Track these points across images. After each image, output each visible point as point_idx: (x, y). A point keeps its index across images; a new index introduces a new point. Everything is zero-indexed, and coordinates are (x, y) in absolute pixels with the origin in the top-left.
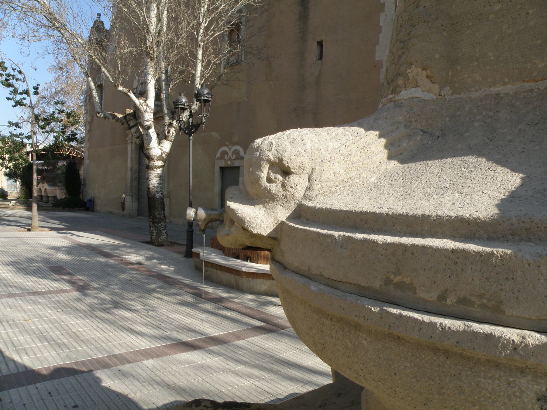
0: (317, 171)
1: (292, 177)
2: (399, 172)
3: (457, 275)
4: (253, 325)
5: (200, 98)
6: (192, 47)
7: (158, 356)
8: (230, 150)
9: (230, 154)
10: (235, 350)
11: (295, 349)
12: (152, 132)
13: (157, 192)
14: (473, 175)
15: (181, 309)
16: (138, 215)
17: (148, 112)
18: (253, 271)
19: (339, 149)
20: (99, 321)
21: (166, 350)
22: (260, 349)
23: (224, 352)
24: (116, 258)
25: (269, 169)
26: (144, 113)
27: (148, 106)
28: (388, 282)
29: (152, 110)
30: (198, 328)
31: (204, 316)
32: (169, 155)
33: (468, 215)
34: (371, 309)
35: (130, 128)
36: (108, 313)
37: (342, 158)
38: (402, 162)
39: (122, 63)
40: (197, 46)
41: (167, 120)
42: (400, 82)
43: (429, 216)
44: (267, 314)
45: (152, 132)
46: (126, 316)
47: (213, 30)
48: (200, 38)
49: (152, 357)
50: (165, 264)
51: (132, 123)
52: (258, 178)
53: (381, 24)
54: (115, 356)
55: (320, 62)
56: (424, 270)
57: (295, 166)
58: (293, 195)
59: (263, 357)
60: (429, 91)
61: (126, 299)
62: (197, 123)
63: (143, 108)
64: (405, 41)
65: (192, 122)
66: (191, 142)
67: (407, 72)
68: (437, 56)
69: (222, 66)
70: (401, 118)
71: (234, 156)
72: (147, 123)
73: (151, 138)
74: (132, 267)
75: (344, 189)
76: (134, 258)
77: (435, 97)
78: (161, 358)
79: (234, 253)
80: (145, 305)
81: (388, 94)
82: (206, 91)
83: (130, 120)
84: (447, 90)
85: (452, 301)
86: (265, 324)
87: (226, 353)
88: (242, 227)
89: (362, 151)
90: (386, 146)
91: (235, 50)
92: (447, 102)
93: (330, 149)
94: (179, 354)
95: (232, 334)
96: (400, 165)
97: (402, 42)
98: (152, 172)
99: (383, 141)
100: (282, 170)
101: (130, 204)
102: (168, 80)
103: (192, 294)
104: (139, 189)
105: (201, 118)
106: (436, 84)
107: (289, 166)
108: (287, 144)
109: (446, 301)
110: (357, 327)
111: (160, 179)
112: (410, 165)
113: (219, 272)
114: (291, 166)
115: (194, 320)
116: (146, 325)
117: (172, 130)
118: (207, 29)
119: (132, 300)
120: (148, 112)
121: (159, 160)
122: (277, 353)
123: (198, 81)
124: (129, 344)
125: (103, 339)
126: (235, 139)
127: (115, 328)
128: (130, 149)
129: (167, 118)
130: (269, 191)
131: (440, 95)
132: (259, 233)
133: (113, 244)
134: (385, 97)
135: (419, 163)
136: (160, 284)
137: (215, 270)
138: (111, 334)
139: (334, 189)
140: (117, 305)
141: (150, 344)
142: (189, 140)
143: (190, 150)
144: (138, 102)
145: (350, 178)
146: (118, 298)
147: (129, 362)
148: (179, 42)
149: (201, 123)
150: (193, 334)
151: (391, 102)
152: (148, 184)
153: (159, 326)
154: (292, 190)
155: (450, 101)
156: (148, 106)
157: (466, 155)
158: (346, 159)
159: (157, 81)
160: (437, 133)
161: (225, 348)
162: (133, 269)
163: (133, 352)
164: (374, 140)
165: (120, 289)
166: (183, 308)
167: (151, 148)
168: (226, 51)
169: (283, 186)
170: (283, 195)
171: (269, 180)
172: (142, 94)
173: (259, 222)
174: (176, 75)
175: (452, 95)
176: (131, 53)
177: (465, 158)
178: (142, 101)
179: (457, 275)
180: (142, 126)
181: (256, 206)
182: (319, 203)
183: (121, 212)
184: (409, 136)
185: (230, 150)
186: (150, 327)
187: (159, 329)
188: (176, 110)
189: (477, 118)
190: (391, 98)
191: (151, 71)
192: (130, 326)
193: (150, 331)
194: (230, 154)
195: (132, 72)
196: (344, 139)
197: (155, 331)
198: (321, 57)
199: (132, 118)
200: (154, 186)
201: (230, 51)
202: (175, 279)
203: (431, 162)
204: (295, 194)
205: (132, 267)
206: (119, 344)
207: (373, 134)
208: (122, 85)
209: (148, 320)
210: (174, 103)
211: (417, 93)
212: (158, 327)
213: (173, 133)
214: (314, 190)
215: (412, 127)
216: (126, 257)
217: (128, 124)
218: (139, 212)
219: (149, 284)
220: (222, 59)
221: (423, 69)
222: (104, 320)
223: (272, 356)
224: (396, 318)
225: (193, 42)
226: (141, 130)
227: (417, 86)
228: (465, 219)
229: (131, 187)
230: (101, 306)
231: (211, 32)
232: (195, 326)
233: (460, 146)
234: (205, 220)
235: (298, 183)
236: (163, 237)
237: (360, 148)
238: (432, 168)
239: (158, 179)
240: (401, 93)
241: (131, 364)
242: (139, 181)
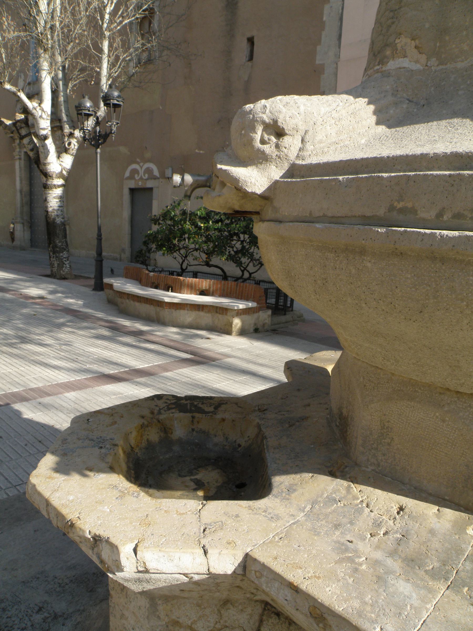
0: (310, 133)
1: (286, 138)
2: (388, 135)
3: (453, 195)
4: (180, 357)
5: (108, 102)
6: (97, 37)
7: (80, 389)
8: (141, 167)
9: (141, 172)
10: (163, 381)
11: (229, 380)
12: (49, 143)
13: (57, 216)
14: (459, 131)
15: (97, 342)
16: (32, 246)
17: (44, 119)
18: (176, 301)
19: (330, 113)
20: (7, 356)
21: (87, 383)
22: (191, 380)
23: (152, 383)
24: (13, 292)
25: (263, 130)
26: (39, 119)
27: (42, 111)
28: (392, 208)
29: (48, 116)
30: (120, 361)
31: (124, 349)
32: (70, 172)
33: (461, 151)
34: (378, 231)
35: (22, 138)
36: (15, 348)
37: (333, 121)
38: (389, 127)
39: (6, 53)
40: (102, 36)
41: (67, 129)
42: (388, 53)
43: (427, 154)
44: (194, 346)
45: (49, 143)
46: (36, 350)
47: (122, 16)
48: (105, 25)
49: (74, 390)
50: (71, 298)
51: (23, 132)
52: (251, 140)
53: (324, 19)
54: (32, 390)
55: (250, 64)
56: (425, 194)
57: (289, 128)
58: (287, 155)
59: (195, 388)
60: (417, 62)
61: (33, 334)
62: (106, 133)
63: (38, 113)
64: (396, 10)
65: (100, 132)
66: (99, 155)
67: (396, 42)
68: (427, 25)
69: (131, 64)
70: (388, 87)
71: (147, 175)
72: (43, 132)
73: (48, 151)
74: (34, 301)
75: (336, 150)
76: (34, 291)
77: (422, 68)
78: (83, 390)
79: (153, 283)
80: (57, 339)
81: (375, 66)
82: (116, 94)
83: (21, 128)
84: (433, 61)
85: (448, 217)
86: (193, 356)
87: (155, 384)
88: (235, 187)
89: (352, 116)
90: (375, 113)
91: (149, 43)
92: (432, 73)
93: (322, 113)
94: (103, 387)
95: (158, 366)
96: (388, 130)
97: (392, 11)
98: (50, 192)
99: (372, 107)
100: (275, 132)
101: (21, 233)
102: (66, 80)
103: (107, 327)
104: (31, 216)
105: (111, 126)
106: (424, 55)
107: (284, 127)
108: (281, 106)
109: (443, 218)
110: (363, 252)
111: (60, 201)
112: (398, 129)
113: (137, 304)
114: (285, 128)
115: (114, 353)
116: (61, 359)
117: (74, 141)
118: (114, 14)
119: (40, 334)
120: (44, 119)
121: (59, 177)
122: (209, 384)
123: (105, 83)
124: (46, 378)
125: (15, 373)
126: (148, 155)
127: (27, 363)
128: (19, 166)
129: (67, 126)
130: (263, 152)
131: (426, 66)
132: (253, 191)
133: (6, 277)
134: (371, 69)
135: (406, 127)
136: (69, 318)
137: (132, 302)
138: (22, 369)
139: (326, 150)
140: (24, 340)
141: (69, 377)
142: (96, 153)
143: (97, 165)
144: (30, 104)
145: (342, 140)
146: (24, 333)
147: (49, 395)
148: (78, 30)
149: (111, 133)
150: (115, 367)
151: (377, 73)
152: (47, 207)
153: (76, 360)
154: (285, 151)
155: (436, 71)
156: (42, 111)
157: (451, 118)
158: (337, 123)
159: (53, 78)
160: (422, 102)
161: (152, 380)
162: (36, 304)
163: (52, 386)
164: (363, 107)
165: (24, 324)
166: (100, 342)
167: (49, 163)
168: (138, 45)
169: (277, 146)
170: (277, 155)
171: (263, 142)
172: (35, 95)
173: (253, 180)
174: (76, 73)
175: (438, 66)
176: (18, 37)
177: (450, 121)
178: (35, 104)
179: (453, 195)
180: (37, 136)
181: (249, 168)
182: (314, 160)
183: (10, 243)
184: (396, 104)
185: (141, 167)
186: (66, 361)
187: (76, 363)
188: (80, 115)
189: (462, 87)
190: (377, 69)
191: (45, 65)
192: (41, 360)
193: (66, 365)
194: (141, 172)
195: (21, 65)
196: (334, 105)
197: (72, 364)
198: (251, 58)
199: (23, 125)
200: (54, 209)
201: (143, 45)
202: (86, 313)
203: (418, 125)
204: (288, 155)
205: (34, 301)
206: (34, 378)
207: (362, 101)
208: (9, 82)
209: (62, 354)
210: (76, 107)
211: (405, 63)
212: (74, 361)
213: (75, 145)
214: (307, 150)
215: (399, 96)
216: (25, 291)
217: (18, 132)
218: (33, 243)
219: (56, 318)
220: (133, 54)
221: (412, 39)
222: (11, 355)
223: (204, 387)
224: (402, 234)
225: (97, 30)
226: (35, 140)
227: (405, 56)
228: (459, 153)
229: (22, 213)
230: (6, 342)
231: (119, 18)
232: (116, 359)
233: (444, 112)
234: (191, 185)
235: (291, 144)
236: (66, 270)
237: (350, 113)
238: (420, 129)
239: (58, 200)
240: (389, 64)
241: (51, 397)
242: (31, 205)
